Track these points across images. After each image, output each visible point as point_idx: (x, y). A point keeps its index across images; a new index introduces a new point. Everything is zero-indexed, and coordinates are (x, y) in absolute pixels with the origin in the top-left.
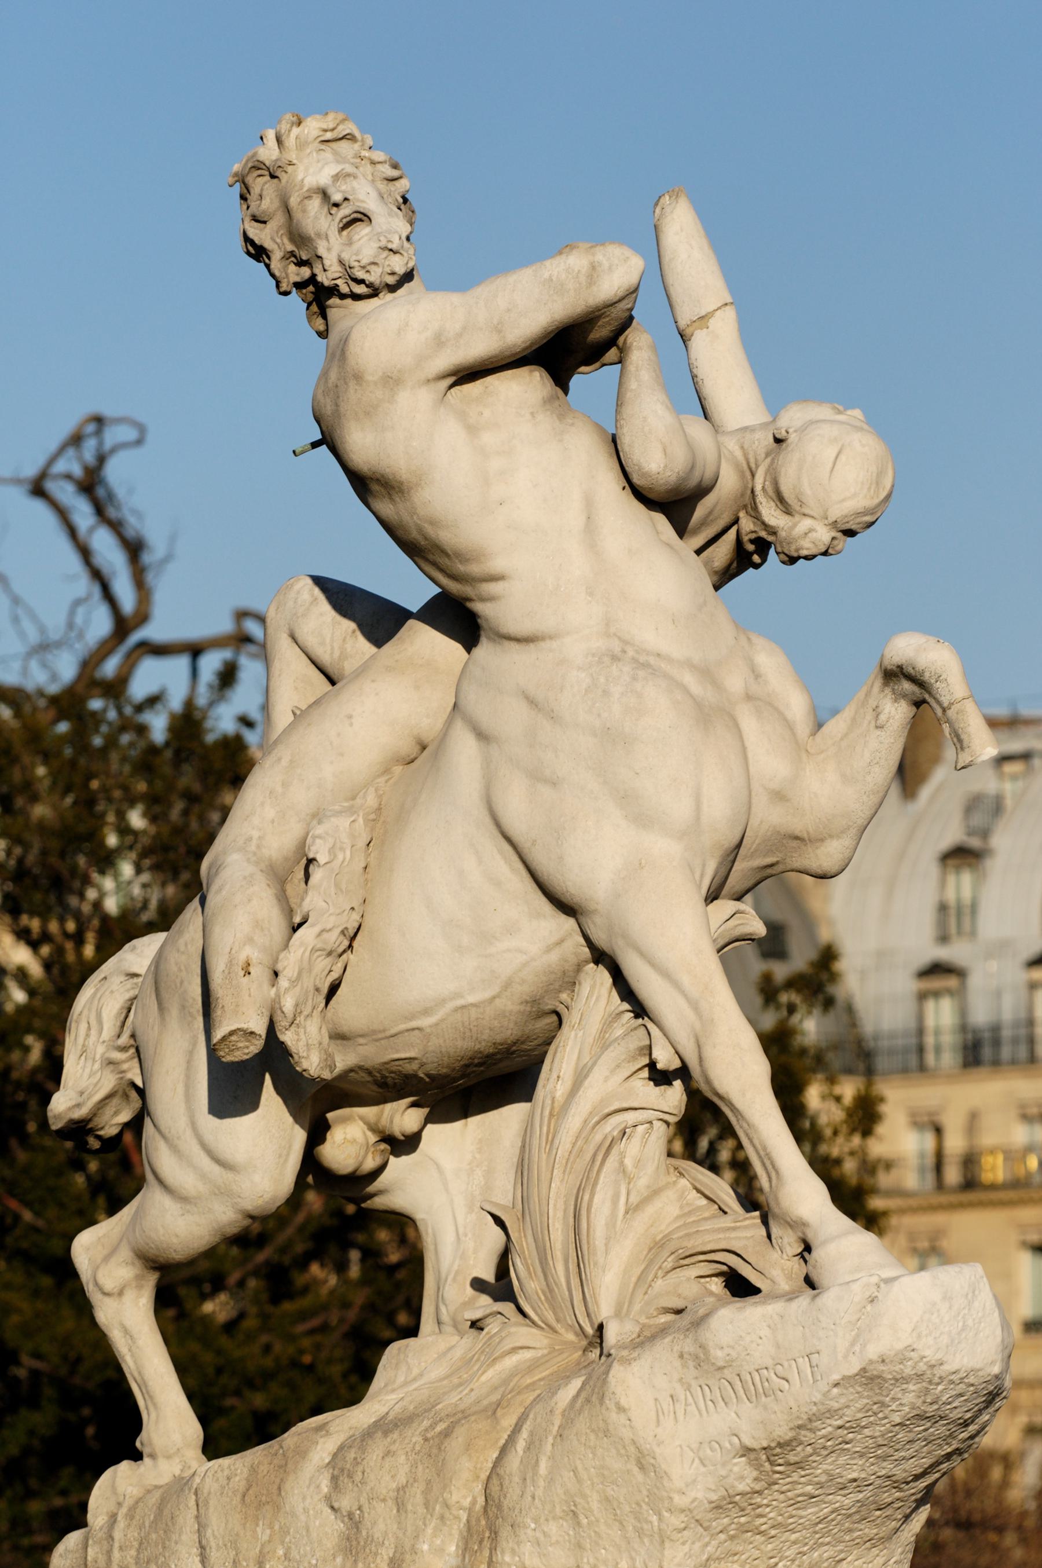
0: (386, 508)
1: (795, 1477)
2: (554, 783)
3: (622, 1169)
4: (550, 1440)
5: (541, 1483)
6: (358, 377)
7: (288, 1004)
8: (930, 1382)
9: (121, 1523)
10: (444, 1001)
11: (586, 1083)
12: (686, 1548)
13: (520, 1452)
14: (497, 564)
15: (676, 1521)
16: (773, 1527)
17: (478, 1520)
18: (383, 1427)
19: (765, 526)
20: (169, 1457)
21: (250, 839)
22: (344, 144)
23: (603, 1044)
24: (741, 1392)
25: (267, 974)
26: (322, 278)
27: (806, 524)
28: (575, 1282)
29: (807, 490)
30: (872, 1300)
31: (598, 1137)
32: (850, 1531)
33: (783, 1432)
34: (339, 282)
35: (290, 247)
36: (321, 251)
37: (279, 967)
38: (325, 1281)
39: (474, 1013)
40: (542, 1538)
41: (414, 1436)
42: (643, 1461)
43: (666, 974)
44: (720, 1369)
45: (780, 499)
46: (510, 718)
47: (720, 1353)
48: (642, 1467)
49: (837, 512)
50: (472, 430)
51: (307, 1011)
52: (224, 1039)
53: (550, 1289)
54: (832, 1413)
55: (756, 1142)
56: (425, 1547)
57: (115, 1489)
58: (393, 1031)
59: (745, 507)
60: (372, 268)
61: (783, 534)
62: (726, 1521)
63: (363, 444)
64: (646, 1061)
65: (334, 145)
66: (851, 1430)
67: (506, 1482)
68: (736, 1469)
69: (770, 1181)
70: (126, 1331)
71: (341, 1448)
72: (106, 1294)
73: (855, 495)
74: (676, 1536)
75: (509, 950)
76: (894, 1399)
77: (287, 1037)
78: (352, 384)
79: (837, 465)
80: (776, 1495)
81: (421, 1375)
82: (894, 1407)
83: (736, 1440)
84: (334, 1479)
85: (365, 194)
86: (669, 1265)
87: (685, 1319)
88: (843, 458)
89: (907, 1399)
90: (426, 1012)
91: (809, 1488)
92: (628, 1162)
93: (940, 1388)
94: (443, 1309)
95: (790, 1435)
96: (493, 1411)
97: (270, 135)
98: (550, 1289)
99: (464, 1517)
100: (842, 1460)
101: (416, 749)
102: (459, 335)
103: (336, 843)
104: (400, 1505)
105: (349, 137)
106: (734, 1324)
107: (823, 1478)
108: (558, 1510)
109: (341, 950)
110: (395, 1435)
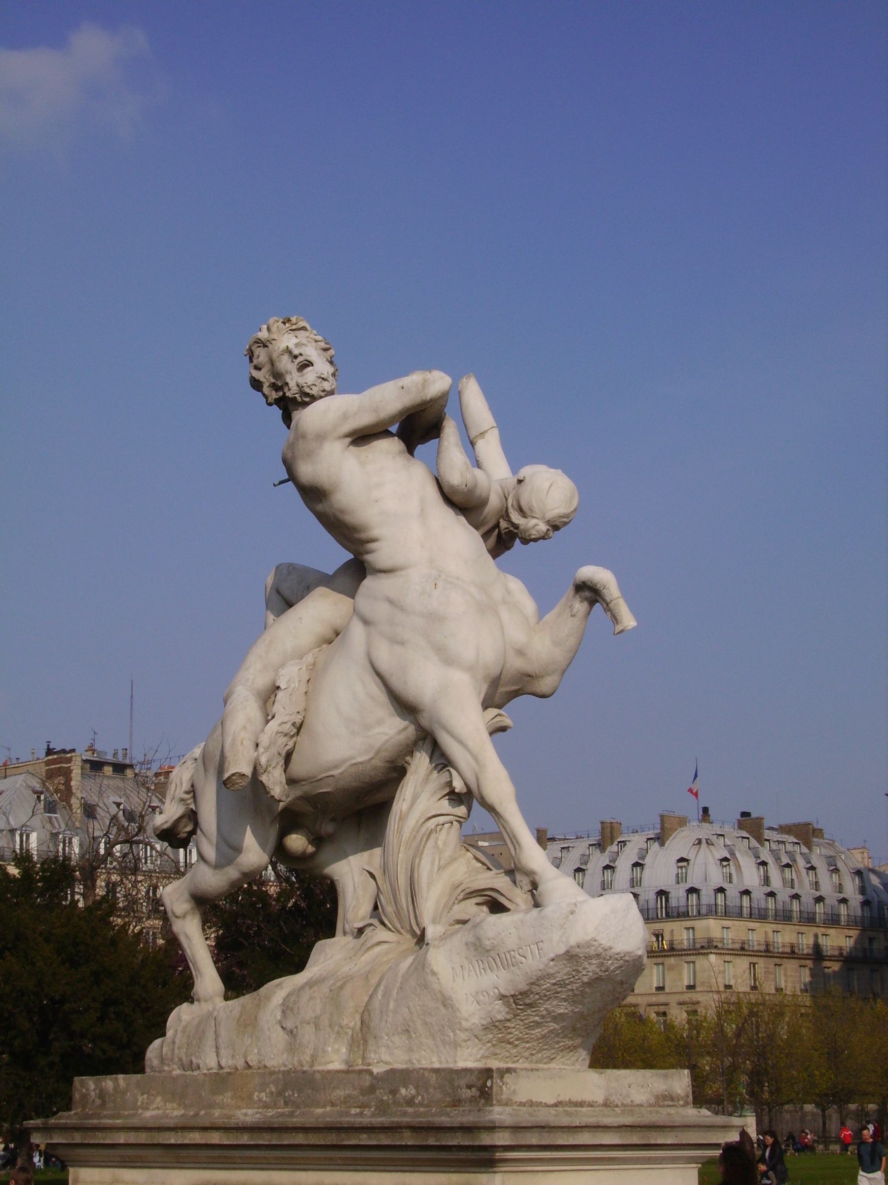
0: (320, 507)
1: (529, 1012)
2: (402, 643)
3: (436, 846)
4: (396, 990)
5: (391, 1014)
6: (304, 436)
7: (263, 760)
8: (604, 959)
9: (179, 1035)
10: (345, 761)
11: (418, 801)
12: (469, 1050)
13: (380, 997)
14: (375, 533)
15: (462, 1036)
16: (517, 1040)
17: (357, 1034)
18: (310, 984)
19: (513, 524)
20: (206, 1001)
21: (248, 680)
22: (302, 332)
23: (426, 780)
24: (499, 964)
25: (253, 746)
26: (288, 394)
27: (533, 522)
28: (411, 907)
29: (535, 504)
30: (572, 912)
31: (424, 829)
32: (558, 1042)
33: (523, 987)
34: (296, 396)
35: (273, 380)
36: (288, 380)
37: (259, 741)
38: (744, 1134)
39: (361, 767)
40: (390, 1044)
41: (325, 989)
42: (446, 1002)
43: (461, 742)
44: (488, 951)
45: (521, 511)
46: (379, 611)
47: (488, 942)
48: (445, 1006)
49: (550, 515)
50: (363, 464)
51: (274, 764)
52: (229, 778)
53: (398, 913)
54: (550, 976)
55: (508, 830)
56: (330, 1049)
57: (182, 1016)
58: (319, 777)
59: (502, 517)
60: (313, 387)
61: (521, 527)
62: (491, 1036)
63: (306, 471)
64: (447, 790)
65: (296, 332)
66: (561, 986)
67: (372, 1015)
68: (497, 1007)
69: (515, 849)
70: (187, 936)
71: (288, 995)
72: (177, 917)
73: (558, 507)
74: (464, 1044)
75: (379, 734)
76: (584, 969)
77: (264, 778)
78: (301, 441)
79: (551, 490)
80: (518, 1022)
81: (332, 957)
82: (584, 973)
83: (496, 991)
84: (283, 1012)
85: (311, 352)
86: (461, 897)
87: (468, 925)
88: (553, 488)
89: (591, 969)
90: (336, 767)
91: (537, 1018)
92: (440, 843)
93: (610, 962)
94: (347, 926)
95: (527, 988)
96: (366, 977)
97: (265, 327)
98: (398, 913)
99: (350, 1033)
100: (555, 1003)
101: (334, 636)
102: (356, 414)
103: (291, 677)
104: (317, 1026)
105: (303, 328)
106: (496, 926)
107: (544, 1013)
108: (400, 1030)
109: (292, 733)
110: (315, 988)
